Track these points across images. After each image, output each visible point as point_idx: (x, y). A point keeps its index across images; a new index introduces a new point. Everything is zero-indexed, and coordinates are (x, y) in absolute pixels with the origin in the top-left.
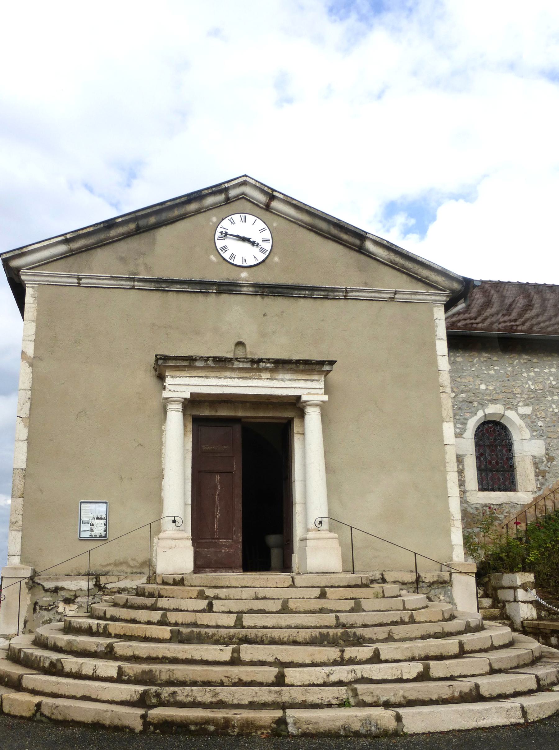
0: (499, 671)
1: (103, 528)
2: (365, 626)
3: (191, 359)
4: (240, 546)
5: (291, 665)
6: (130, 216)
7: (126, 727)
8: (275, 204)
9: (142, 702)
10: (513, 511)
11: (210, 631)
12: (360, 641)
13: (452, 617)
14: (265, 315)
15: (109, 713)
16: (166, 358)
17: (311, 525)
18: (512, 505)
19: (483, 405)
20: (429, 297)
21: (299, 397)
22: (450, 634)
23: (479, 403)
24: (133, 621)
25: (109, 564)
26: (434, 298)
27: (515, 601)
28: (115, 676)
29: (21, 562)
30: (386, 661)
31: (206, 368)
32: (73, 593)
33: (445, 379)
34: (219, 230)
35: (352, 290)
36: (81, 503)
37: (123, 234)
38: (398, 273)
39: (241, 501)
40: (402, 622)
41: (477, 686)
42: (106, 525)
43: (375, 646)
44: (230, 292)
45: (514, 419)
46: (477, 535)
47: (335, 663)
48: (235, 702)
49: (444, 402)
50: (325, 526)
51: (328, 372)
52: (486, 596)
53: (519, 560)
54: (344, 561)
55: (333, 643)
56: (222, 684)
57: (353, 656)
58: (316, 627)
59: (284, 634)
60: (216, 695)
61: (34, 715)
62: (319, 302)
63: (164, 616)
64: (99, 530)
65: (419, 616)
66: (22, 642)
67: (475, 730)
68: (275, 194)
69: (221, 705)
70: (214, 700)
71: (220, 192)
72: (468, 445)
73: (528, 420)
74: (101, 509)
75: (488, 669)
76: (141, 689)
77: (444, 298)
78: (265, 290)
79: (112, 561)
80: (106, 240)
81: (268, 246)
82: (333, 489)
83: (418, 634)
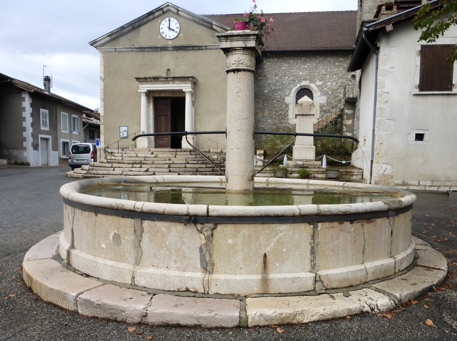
3: (146, 78)
8: (179, 13)
14: (177, 58)
19: (300, 81)
23: (298, 81)
31: (151, 81)
35: (208, 46)
62: (197, 51)
64: (125, 135)
68: (179, 9)
73: (320, 88)
74: (126, 128)
81: (178, 30)
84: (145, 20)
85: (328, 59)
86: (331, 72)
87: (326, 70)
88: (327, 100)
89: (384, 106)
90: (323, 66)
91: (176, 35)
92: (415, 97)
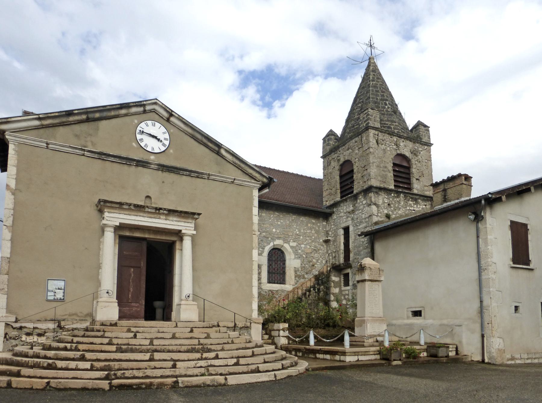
0: (268, 362)
1: (62, 294)
2: (211, 344)
3: (121, 204)
4: (143, 307)
5: (179, 360)
6: (83, 111)
7: (100, 388)
8: (172, 119)
9: (107, 378)
10: (283, 294)
11: (138, 347)
12: (209, 351)
13: (250, 342)
14: (163, 182)
15: (91, 383)
16: (106, 201)
17: (183, 297)
18: (283, 291)
19: (273, 240)
20: (251, 184)
21: (181, 231)
22: (249, 348)
23: (272, 239)
24: (92, 343)
25: (66, 315)
26: (253, 184)
27: (279, 336)
28: (89, 368)
29: (7, 313)
30: (221, 359)
31: (130, 209)
32: (43, 331)
33: (256, 227)
34: (139, 128)
35: (212, 175)
36: (48, 280)
37: (78, 120)
38: (237, 169)
39: (145, 283)
40: (228, 343)
41: (258, 367)
42: (64, 293)
43: (216, 353)
44: (144, 166)
45: (287, 248)
46: (265, 305)
47: (199, 359)
48: (154, 376)
49: (254, 239)
50: (191, 298)
51: (197, 219)
52: (266, 334)
53: (283, 318)
54: (199, 316)
55: (198, 352)
56: (146, 369)
57: (207, 356)
58: (189, 345)
59: (175, 348)
60: (145, 373)
61: (45, 387)
62: (194, 179)
63: (111, 340)
64: (60, 295)
65: (235, 341)
66: (8, 356)
67: (256, 382)
68: (173, 113)
69: (147, 377)
70: (144, 375)
71: (141, 106)
72: (264, 260)
74: (61, 284)
75: (263, 361)
76: (106, 373)
77: (259, 186)
78: (163, 168)
79: (67, 313)
80: (66, 122)
81: (167, 143)
82: (195, 280)
83: (235, 348)
84: (113, 113)
85: (301, 219)
86: (305, 233)
87: (300, 231)
88: (301, 264)
89: (494, 276)
90: (297, 225)
91: (163, 149)
92: (511, 269)
